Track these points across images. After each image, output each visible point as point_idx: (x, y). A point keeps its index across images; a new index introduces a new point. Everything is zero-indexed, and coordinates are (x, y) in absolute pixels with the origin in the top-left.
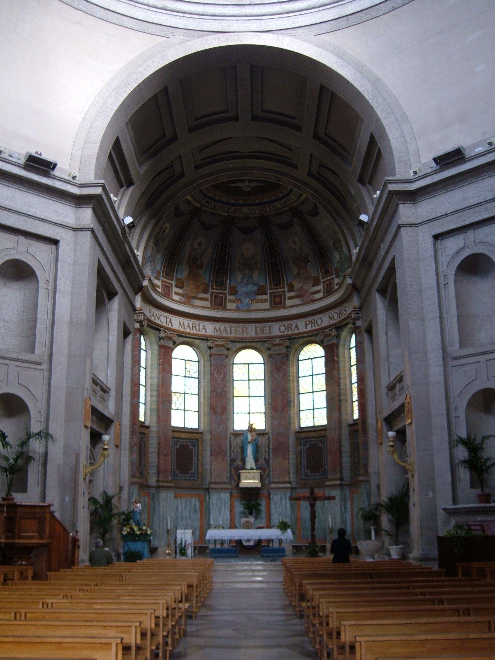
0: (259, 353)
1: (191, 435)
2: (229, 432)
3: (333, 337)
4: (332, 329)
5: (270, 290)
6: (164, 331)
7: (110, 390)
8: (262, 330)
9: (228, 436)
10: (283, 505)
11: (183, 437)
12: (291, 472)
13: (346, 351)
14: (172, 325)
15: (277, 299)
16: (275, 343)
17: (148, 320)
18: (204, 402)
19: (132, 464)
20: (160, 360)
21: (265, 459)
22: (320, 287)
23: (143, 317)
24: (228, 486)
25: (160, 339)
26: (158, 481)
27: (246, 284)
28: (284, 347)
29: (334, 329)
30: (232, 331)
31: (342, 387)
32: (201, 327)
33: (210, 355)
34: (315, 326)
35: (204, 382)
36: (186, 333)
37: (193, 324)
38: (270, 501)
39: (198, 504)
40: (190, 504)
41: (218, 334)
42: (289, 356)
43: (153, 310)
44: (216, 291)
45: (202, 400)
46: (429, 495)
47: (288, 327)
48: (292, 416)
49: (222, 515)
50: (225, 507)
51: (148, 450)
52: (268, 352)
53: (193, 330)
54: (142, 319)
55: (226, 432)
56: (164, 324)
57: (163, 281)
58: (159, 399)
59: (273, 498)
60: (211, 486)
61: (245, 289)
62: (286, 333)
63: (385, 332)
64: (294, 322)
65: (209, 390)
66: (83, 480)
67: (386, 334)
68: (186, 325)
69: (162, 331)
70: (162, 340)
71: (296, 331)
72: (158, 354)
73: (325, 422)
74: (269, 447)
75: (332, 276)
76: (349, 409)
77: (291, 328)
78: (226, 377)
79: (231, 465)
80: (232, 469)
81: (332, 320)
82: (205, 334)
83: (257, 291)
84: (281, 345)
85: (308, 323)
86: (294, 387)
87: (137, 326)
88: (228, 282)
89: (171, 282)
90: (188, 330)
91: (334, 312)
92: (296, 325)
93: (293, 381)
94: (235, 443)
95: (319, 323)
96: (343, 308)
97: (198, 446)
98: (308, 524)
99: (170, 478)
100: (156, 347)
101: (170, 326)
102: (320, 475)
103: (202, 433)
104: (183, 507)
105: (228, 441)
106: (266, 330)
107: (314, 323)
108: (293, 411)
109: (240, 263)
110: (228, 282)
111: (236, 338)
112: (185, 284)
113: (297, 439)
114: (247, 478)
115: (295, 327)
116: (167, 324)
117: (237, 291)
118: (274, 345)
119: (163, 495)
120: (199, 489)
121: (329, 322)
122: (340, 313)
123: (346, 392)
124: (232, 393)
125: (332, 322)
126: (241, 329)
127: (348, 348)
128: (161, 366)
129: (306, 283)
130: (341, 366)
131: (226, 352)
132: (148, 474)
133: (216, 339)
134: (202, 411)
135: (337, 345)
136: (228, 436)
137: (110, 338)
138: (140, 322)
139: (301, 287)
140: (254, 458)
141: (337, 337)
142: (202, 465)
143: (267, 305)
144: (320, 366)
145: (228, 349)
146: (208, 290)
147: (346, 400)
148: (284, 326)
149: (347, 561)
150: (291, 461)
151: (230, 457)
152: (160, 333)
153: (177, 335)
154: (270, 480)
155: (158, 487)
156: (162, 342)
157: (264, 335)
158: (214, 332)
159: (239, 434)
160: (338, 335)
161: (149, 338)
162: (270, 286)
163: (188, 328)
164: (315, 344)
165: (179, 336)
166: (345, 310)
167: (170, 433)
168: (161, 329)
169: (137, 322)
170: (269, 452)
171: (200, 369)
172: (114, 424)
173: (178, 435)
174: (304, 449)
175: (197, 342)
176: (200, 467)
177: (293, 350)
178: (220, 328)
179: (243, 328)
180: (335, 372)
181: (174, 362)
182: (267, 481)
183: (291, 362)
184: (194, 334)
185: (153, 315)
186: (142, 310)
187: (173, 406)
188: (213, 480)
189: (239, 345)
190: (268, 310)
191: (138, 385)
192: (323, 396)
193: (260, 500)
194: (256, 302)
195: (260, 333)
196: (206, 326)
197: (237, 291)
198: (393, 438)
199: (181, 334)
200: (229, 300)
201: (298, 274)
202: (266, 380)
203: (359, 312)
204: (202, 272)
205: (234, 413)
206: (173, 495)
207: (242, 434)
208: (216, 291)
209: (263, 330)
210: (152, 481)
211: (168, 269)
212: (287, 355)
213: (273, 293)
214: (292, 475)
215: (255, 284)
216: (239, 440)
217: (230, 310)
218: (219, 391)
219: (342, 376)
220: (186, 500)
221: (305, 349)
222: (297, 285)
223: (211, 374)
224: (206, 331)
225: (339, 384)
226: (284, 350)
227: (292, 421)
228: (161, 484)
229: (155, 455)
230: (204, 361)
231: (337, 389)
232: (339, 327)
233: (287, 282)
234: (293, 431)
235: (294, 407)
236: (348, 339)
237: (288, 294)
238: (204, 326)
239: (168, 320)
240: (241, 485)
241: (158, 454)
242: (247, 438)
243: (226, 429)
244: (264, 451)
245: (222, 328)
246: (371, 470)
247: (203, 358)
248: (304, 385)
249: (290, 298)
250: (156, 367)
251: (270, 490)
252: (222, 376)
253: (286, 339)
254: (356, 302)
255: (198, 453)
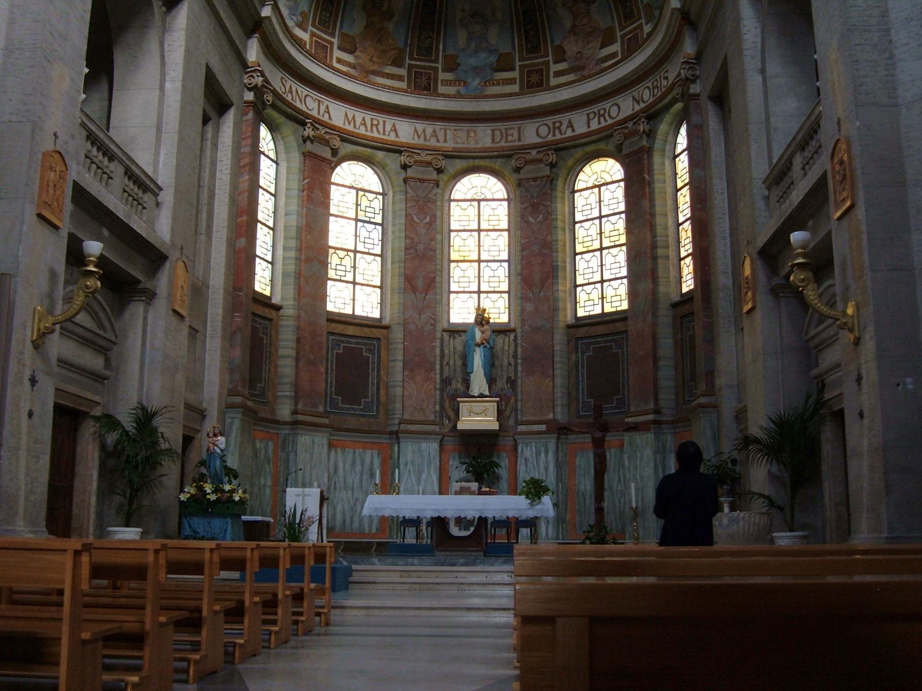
0: (499, 180)
1: (367, 330)
2: (439, 327)
3: (641, 137)
4: (640, 119)
5: (520, 61)
6: (312, 124)
7: (160, 189)
8: (505, 135)
9: (438, 335)
10: (542, 465)
11: (350, 333)
12: (559, 402)
13: (667, 163)
14: (330, 118)
15: (534, 78)
16: (528, 157)
17: (275, 93)
18: (392, 269)
19: (230, 368)
20: (304, 180)
21: (509, 378)
22: (616, 47)
23: (261, 79)
24: (436, 428)
25: (305, 141)
26: (295, 412)
27: (476, 51)
28: (547, 165)
29: (643, 120)
30: (448, 137)
31: (659, 231)
32: (388, 127)
33: (405, 181)
34: (606, 121)
35: (393, 232)
36: (358, 136)
37: (372, 119)
38: (516, 457)
39: (377, 463)
40: (363, 461)
41: (421, 141)
42: (555, 182)
43: (289, 83)
44: (418, 63)
45: (389, 266)
46: (905, 384)
47: (555, 128)
48: (561, 294)
49: (423, 483)
50: (429, 467)
51: (277, 352)
52: (516, 176)
53: (372, 131)
54: (260, 84)
55: (434, 325)
56: (314, 113)
57: (313, 35)
58: (301, 254)
59: (522, 450)
60: (403, 427)
61: (472, 61)
62: (550, 138)
63: (760, 67)
64: (565, 118)
65: (403, 245)
66: (29, 346)
67: (763, 71)
68: (359, 120)
69: (309, 125)
70: (308, 142)
71: (569, 133)
72: (300, 170)
73: (625, 306)
74: (515, 357)
75: (640, 22)
76: (673, 273)
77: (559, 128)
78: (435, 221)
79: (442, 390)
80: (446, 397)
81: (638, 103)
82: (396, 139)
83: (495, 65)
84: (540, 161)
85: (592, 116)
86: (565, 242)
87: (250, 96)
88: (441, 47)
89: (332, 39)
90: (362, 131)
91: (641, 90)
92: (570, 121)
93: (564, 230)
94: (452, 349)
95: (614, 114)
96: (662, 74)
97: (379, 352)
98: (590, 503)
99: (321, 409)
100: (296, 156)
101: (326, 118)
102: (613, 408)
103: (387, 328)
104: (348, 466)
105: (438, 343)
106: (512, 135)
107: (603, 115)
108: (563, 287)
109: (463, 11)
110: (441, 47)
111: (455, 150)
112: (358, 45)
113: (569, 342)
114: (471, 413)
115: (568, 127)
116: (319, 113)
117: (459, 65)
118: (526, 163)
119: (304, 439)
120: (379, 432)
121: (633, 109)
122: (654, 88)
123: (668, 241)
124: (446, 253)
125: (637, 108)
126: (465, 133)
127: (672, 156)
128: (306, 192)
129: (588, 43)
130: (656, 191)
131: (434, 176)
132: (276, 397)
133: (417, 151)
134: (389, 286)
135: (649, 151)
136: (438, 335)
137: (168, 85)
138: (254, 88)
139: (578, 53)
140: (485, 374)
141: (648, 136)
142: (387, 387)
143: (515, 88)
144: (616, 197)
145: (440, 171)
146: (403, 60)
147: (667, 257)
148: (547, 125)
149: (707, 538)
150: (558, 381)
151: (441, 375)
152: (305, 130)
153: (339, 136)
154: (516, 419)
155: (295, 423)
156: (309, 146)
157: (508, 144)
158: (413, 139)
159: (458, 332)
160: (650, 131)
161: (283, 138)
162: (521, 54)
163: (363, 128)
164: (606, 159)
165: (343, 140)
166: (666, 78)
167: (323, 321)
168: (307, 121)
169: (250, 89)
170: (516, 364)
171: (386, 208)
172: (168, 265)
173: (339, 328)
174: (583, 359)
175: (380, 155)
176: (382, 392)
177: (564, 171)
178: (424, 131)
179: (468, 132)
180: (646, 203)
181: (335, 192)
182: (511, 422)
183: (559, 194)
184: (373, 139)
185: (291, 92)
186: (259, 66)
187: (331, 274)
188: (406, 417)
189: (460, 164)
190: (516, 94)
191: (253, 221)
192: (621, 255)
193: (498, 457)
194: (494, 85)
195: (501, 140)
196: (397, 127)
197: (459, 65)
198: (803, 247)
199: (347, 138)
200: (442, 80)
201: (574, 26)
202: (512, 230)
203: (696, 67)
204: (390, 26)
205: (450, 292)
206: (325, 441)
207: (465, 331)
208: (418, 63)
209: (507, 135)
210: (284, 411)
211: (323, 12)
212: (551, 181)
213: (526, 66)
214: (559, 409)
215: (491, 52)
216: (458, 343)
217: (443, 95)
218: (421, 247)
219: (658, 209)
220: (354, 453)
221: (587, 169)
222: (572, 48)
223: (406, 215)
224: (397, 136)
225: (652, 227)
226: (547, 171)
227: (561, 304)
228: (300, 418)
229: (290, 362)
230: (394, 193)
231: (649, 236)
232: (652, 115)
233: (552, 43)
234: (562, 324)
235: (565, 278)
236: (670, 138)
237: (554, 68)
238: (394, 125)
239: (323, 108)
240: (460, 426)
241: (297, 360)
242: (473, 336)
243: (434, 321)
244: (506, 362)
245: (429, 130)
246: (721, 381)
247: (393, 187)
248: (585, 235)
249: (558, 74)
250: (295, 192)
251: (516, 437)
252: (428, 220)
253: (550, 150)
254: (689, 48)
255: (379, 365)
